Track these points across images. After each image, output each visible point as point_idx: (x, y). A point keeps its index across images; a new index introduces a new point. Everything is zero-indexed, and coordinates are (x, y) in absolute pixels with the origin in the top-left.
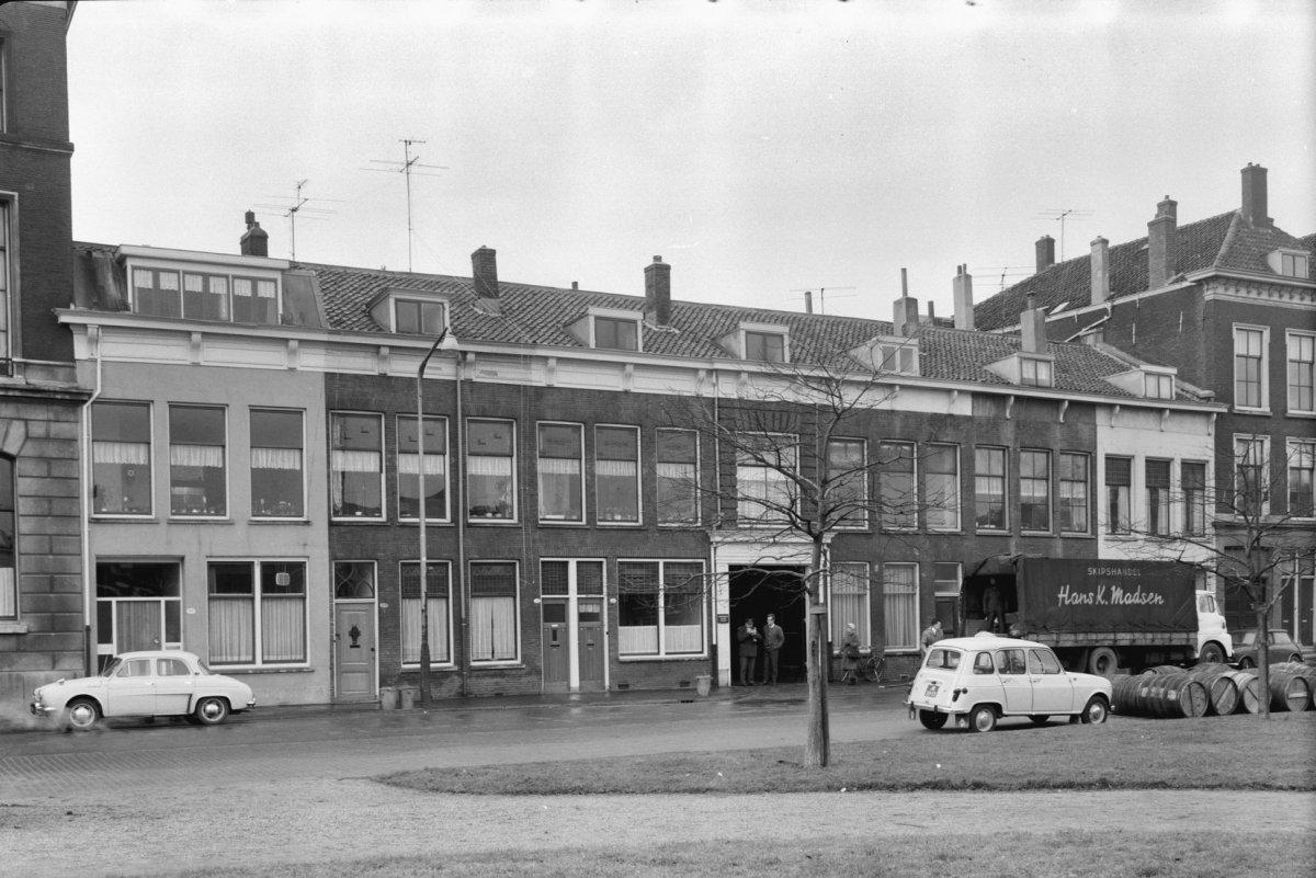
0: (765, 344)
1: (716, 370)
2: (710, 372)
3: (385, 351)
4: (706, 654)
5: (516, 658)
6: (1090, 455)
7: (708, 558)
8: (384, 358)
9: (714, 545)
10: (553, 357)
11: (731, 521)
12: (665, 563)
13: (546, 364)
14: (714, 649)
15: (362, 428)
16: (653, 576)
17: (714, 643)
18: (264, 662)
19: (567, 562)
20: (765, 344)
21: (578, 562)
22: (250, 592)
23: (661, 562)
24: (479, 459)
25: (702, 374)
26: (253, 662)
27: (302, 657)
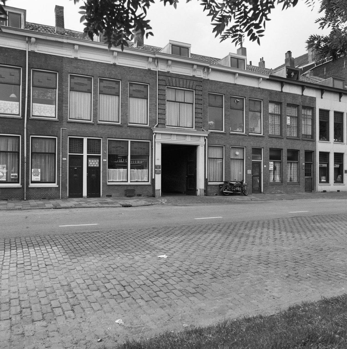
0: (180, 50)
1: (157, 58)
2: (154, 59)
3: (170, 62)
4: (149, 183)
5: (148, 182)
6: (313, 109)
7: (152, 140)
8: (195, 70)
9: (155, 134)
10: (238, 73)
11: (162, 124)
12: (131, 141)
13: (193, 67)
14: (153, 181)
15: (10, 74)
16: (71, 146)
17: (153, 178)
18: (131, 182)
19: (83, 139)
20: (180, 50)
21: (88, 139)
22: (280, 160)
23: (129, 141)
24: (105, 96)
25: (150, 60)
26: (127, 182)
27: (126, 180)
